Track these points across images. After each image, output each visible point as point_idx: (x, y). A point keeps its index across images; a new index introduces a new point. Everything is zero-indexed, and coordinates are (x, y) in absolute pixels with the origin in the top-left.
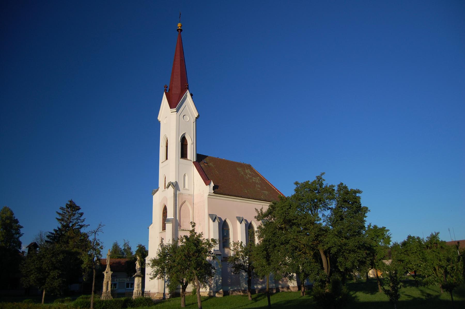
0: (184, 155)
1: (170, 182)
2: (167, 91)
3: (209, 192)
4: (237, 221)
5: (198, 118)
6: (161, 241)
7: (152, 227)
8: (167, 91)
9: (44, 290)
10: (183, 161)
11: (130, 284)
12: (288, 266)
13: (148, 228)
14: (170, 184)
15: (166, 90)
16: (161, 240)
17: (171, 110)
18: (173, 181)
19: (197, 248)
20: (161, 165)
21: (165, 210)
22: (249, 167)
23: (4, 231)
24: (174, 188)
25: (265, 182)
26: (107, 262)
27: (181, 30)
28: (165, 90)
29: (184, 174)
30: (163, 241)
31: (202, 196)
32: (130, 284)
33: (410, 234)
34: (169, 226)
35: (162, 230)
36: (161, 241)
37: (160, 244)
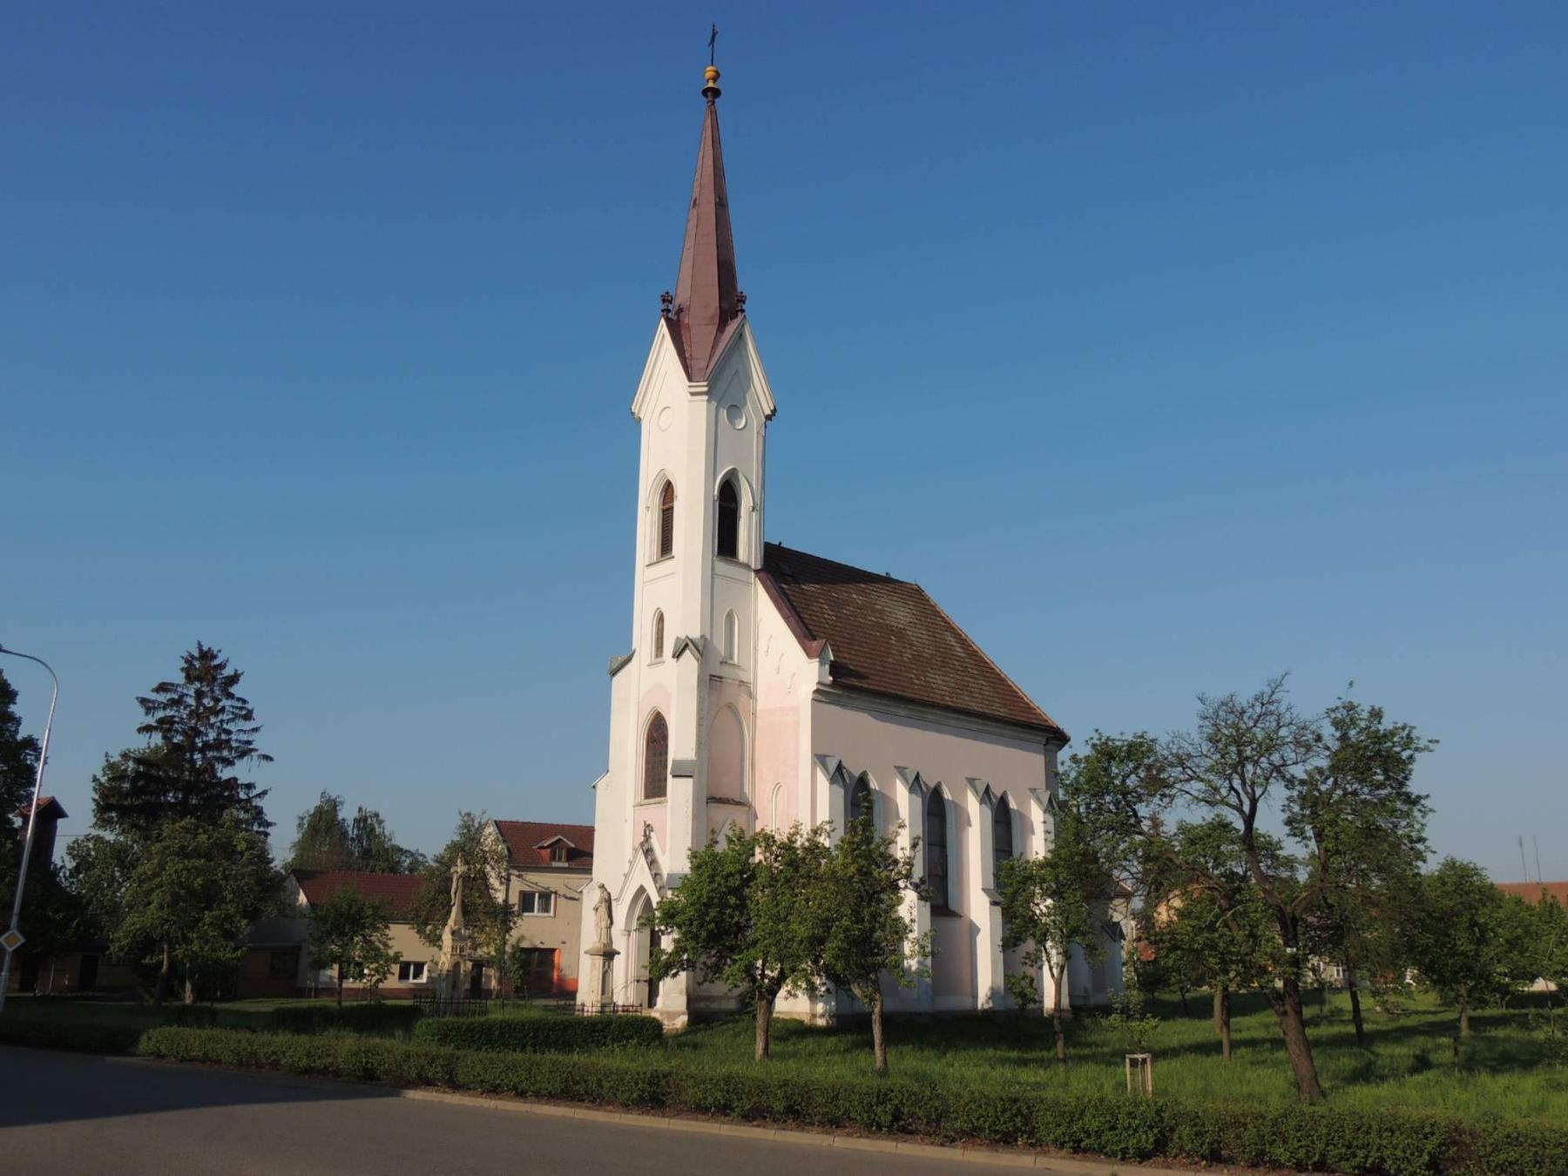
0: (726, 543)
1: (687, 637)
2: (670, 315)
3: (817, 681)
4: (898, 781)
5: (773, 418)
6: (645, 835)
7: (608, 785)
8: (670, 315)
9: (188, 986)
10: (722, 567)
11: (412, 968)
12: (1253, 942)
13: (594, 787)
14: (687, 645)
15: (669, 311)
16: (645, 831)
17: (690, 387)
18: (695, 634)
19: (1371, 915)
20: (642, 574)
21: (657, 733)
22: (915, 595)
23: (1230, 892)
24: (698, 660)
25: (970, 648)
26: (453, 896)
27: (716, 93)
28: (663, 311)
29: (726, 613)
30: (650, 837)
31: (789, 692)
32: (412, 968)
33: (245, 674)
34: (680, 792)
35: (643, 797)
36: (643, 833)
37: (642, 844)
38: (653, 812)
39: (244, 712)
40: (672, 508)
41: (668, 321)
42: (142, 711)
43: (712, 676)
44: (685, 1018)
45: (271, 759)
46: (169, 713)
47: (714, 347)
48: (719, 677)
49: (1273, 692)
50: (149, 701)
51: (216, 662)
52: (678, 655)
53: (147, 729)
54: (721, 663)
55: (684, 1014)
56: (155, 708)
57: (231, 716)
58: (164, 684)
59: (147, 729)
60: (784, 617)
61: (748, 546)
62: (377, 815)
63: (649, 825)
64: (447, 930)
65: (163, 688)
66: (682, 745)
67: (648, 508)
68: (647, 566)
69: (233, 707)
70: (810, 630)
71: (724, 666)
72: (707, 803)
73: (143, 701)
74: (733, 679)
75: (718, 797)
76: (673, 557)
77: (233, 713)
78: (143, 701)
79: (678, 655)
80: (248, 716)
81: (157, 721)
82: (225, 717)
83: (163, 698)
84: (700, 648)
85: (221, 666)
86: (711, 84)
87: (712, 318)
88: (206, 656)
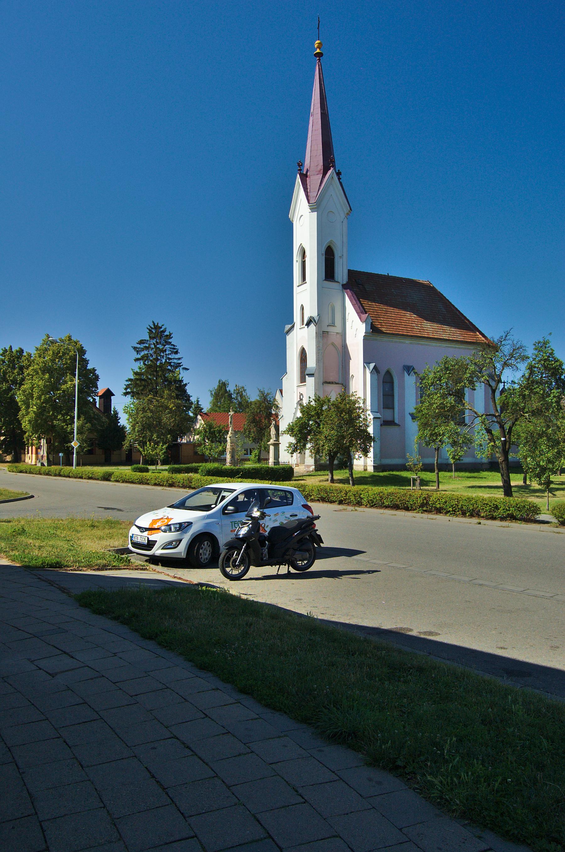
20: (296, 290)
38: (303, 390)
39: (175, 351)
40: (305, 261)
41: (300, 174)
42: (135, 353)
43: (323, 332)
44: (314, 467)
45: (188, 369)
46: (146, 352)
47: (320, 186)
48: (327, 332)
49: (506, 336)
50: (137, 348)
51: (162, 330)
52: (308, 324)
53: (137, 360)
54: (328, 326)
55: (313, 465)
56: (140, 351)
57: (170, 352)
58: (142, 340)
59: (137, 360)
60: (353, 305)
61: (341, 274)
62: (243, 387)
63: (302, 394)
64: (228, 436)
65: (141, 342)
66: (311, 363)
67: (297, 261)
68: (298, 286)
69: (171, 348)
70: (364, 309)
71: (329, 327)
72: (323, 384)
73: (135, 348)
74: (333, 332)
75: (328, 381)
76: (306, 283)
77: (170, 351)
78: (135, 348)
79: (308, 324)
80: (176, 353)
81: (141, 357)
82: (167, 353)
83: (142, 346)
84: (317, 321)
85: (164, 331)
86: (318, 51)
87: (320, 171)
88: (157, 327)
